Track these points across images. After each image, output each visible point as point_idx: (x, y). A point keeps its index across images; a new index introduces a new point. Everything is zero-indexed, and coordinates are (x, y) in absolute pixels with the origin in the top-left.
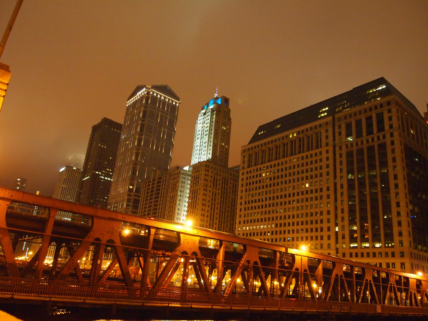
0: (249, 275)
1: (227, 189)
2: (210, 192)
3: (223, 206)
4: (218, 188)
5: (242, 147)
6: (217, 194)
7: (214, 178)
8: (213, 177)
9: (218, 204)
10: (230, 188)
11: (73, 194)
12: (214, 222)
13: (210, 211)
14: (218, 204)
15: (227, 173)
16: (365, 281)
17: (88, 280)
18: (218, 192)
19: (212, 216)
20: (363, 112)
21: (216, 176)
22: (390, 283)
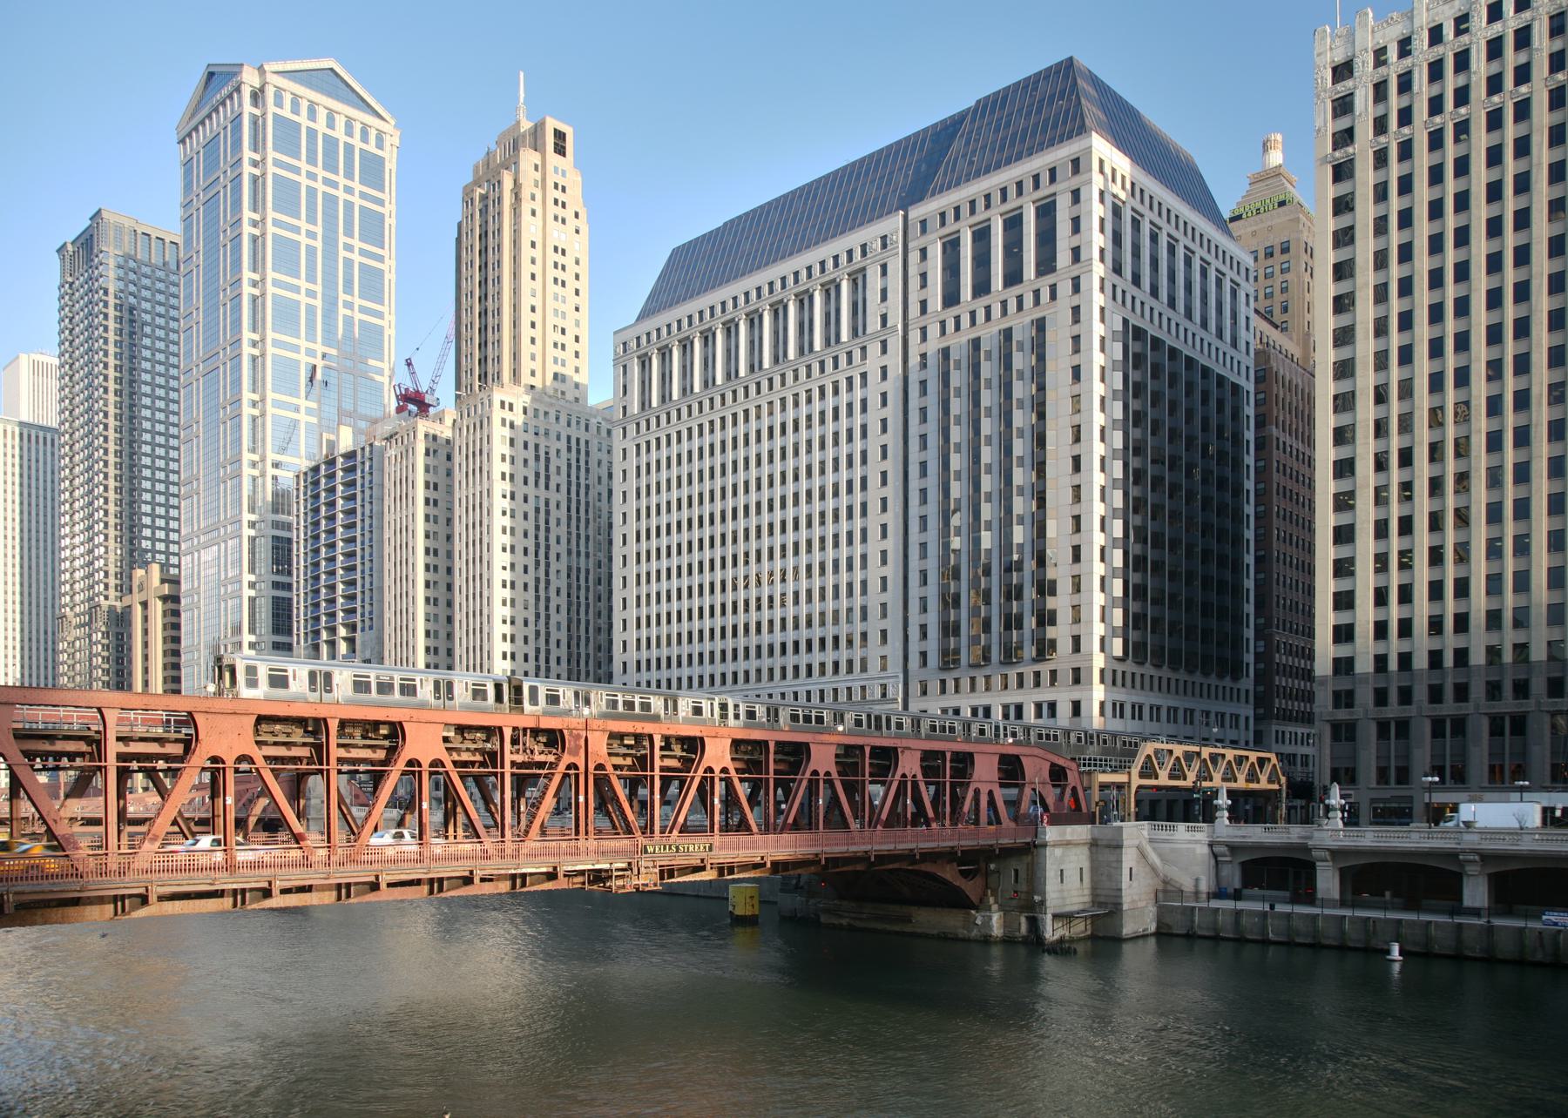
0: (622, 740)
1: (587, 453)
2: (526, 500)
3: (587, 547)
4: (553, 485)
5: (615, 333)
6: (553, 506)
7: (537, 446)
8: (531, 447)
9: (558, 473)
10: (599, 482)
11: (45, 476)
12: (553, 622)
13: (531, 569)
14: (558, 473)
15: (583, 427)
16: (808, 775)
17: (382, 747)
18: (554, 497)
19: (542, 585)
20: (1028, 185)
21: (543, 443)
22: (811, 767)
